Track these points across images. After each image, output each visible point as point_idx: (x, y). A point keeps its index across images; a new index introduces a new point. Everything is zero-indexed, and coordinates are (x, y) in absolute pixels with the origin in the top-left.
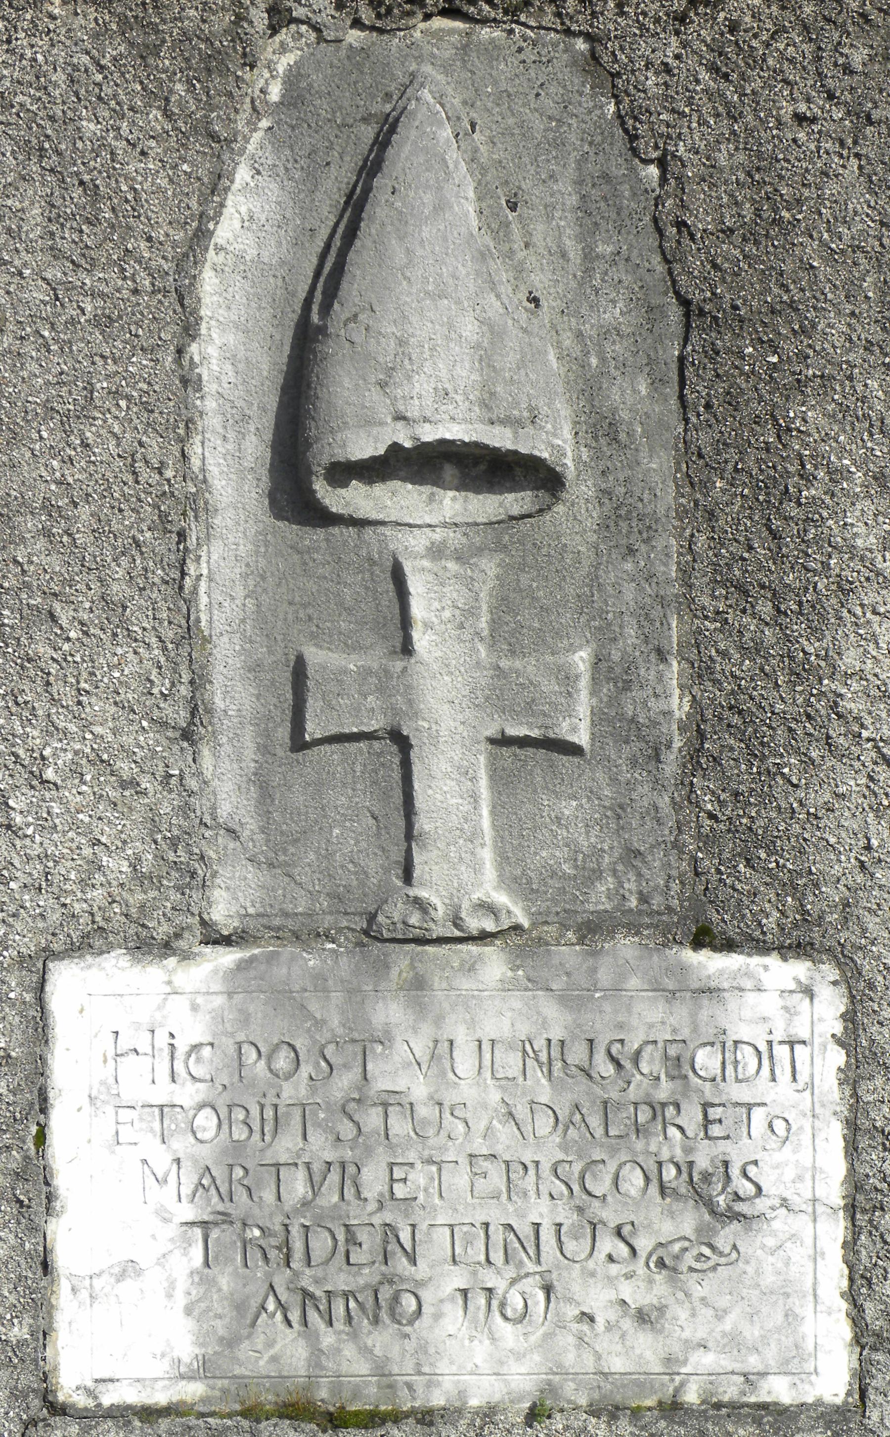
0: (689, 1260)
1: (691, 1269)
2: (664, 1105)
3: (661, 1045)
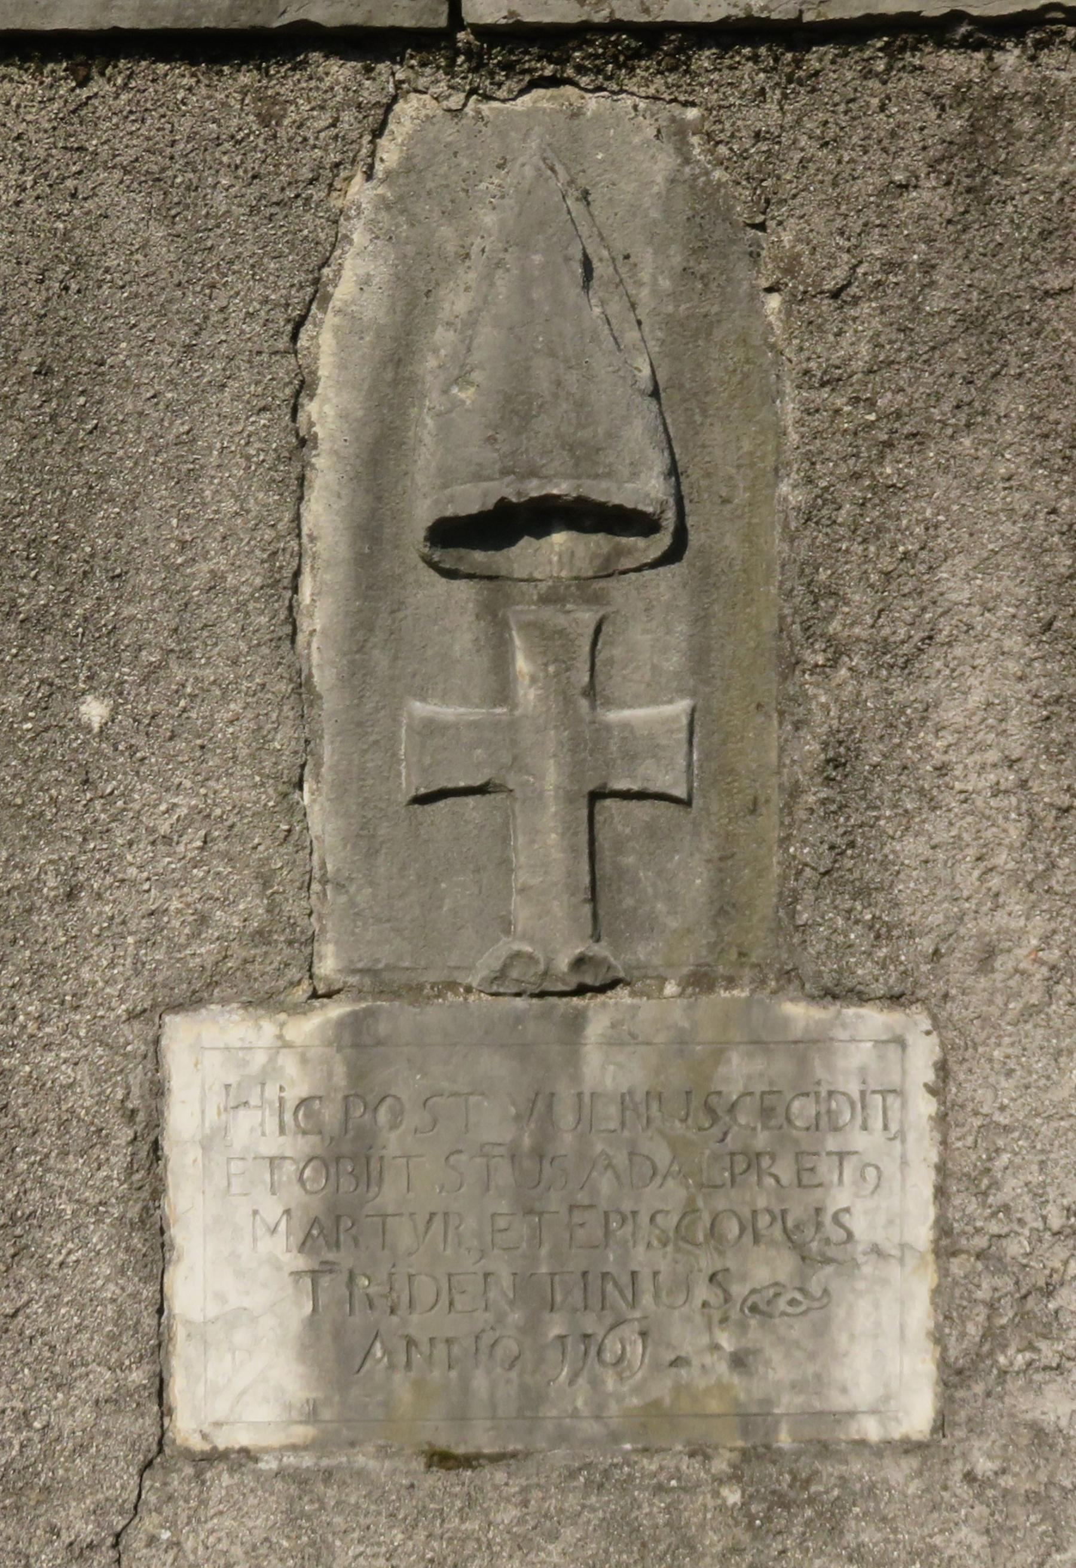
0: (782, 1304)
1: (784, 1314)
2: (758, 1155)
3: (758, 1097)
